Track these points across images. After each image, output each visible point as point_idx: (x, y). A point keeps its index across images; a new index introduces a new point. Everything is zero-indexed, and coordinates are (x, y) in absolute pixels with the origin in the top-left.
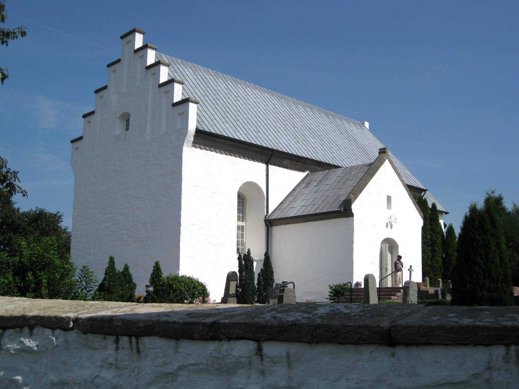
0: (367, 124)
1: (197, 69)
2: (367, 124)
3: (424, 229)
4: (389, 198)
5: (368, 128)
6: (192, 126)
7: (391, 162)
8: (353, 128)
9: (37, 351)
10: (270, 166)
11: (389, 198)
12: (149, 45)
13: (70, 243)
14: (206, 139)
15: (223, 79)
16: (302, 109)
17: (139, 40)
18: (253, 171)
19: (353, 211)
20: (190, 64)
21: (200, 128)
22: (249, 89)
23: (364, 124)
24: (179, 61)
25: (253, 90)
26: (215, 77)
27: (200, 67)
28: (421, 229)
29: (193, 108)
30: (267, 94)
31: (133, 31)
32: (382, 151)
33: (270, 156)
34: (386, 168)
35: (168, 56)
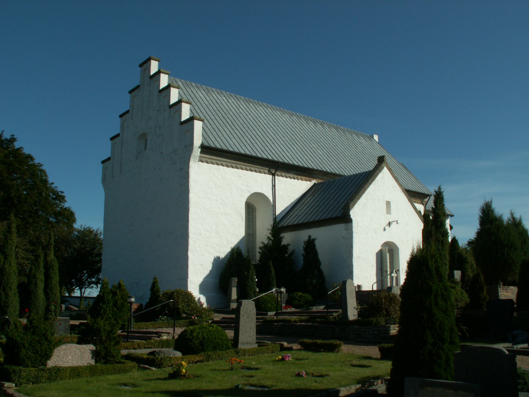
0: (376, 137)
1: (210, 91)
2: (376, 137)
3: (424, 231)
4: (388, 204)
5: (377, 141)
6: (198, 141)
7: (390, 169)
8: (363, 140)
9: (45, 365)
10: (276, 177)
11: (388, 204)
12: (162, 70)
13: (100, 261)
14: (210, 152)
15: (236, 99)
16: (312, 125)
17: (154, 66)
18: (259, 182)
19: (351, 217)
20: (204, 87)
21: (206, 144)
22: (261, 108)
23: (372, 137)
24: (193, 84)
25: (256, 106)
26: (228, 98)
27: (214, 89)
28: (421, 232)
29: (198, 125)
30: (278, 113)
31: (149, 60)
32: (381, 160)
33: (275, 167)
34: (385, 175)
35: (183, 81)
